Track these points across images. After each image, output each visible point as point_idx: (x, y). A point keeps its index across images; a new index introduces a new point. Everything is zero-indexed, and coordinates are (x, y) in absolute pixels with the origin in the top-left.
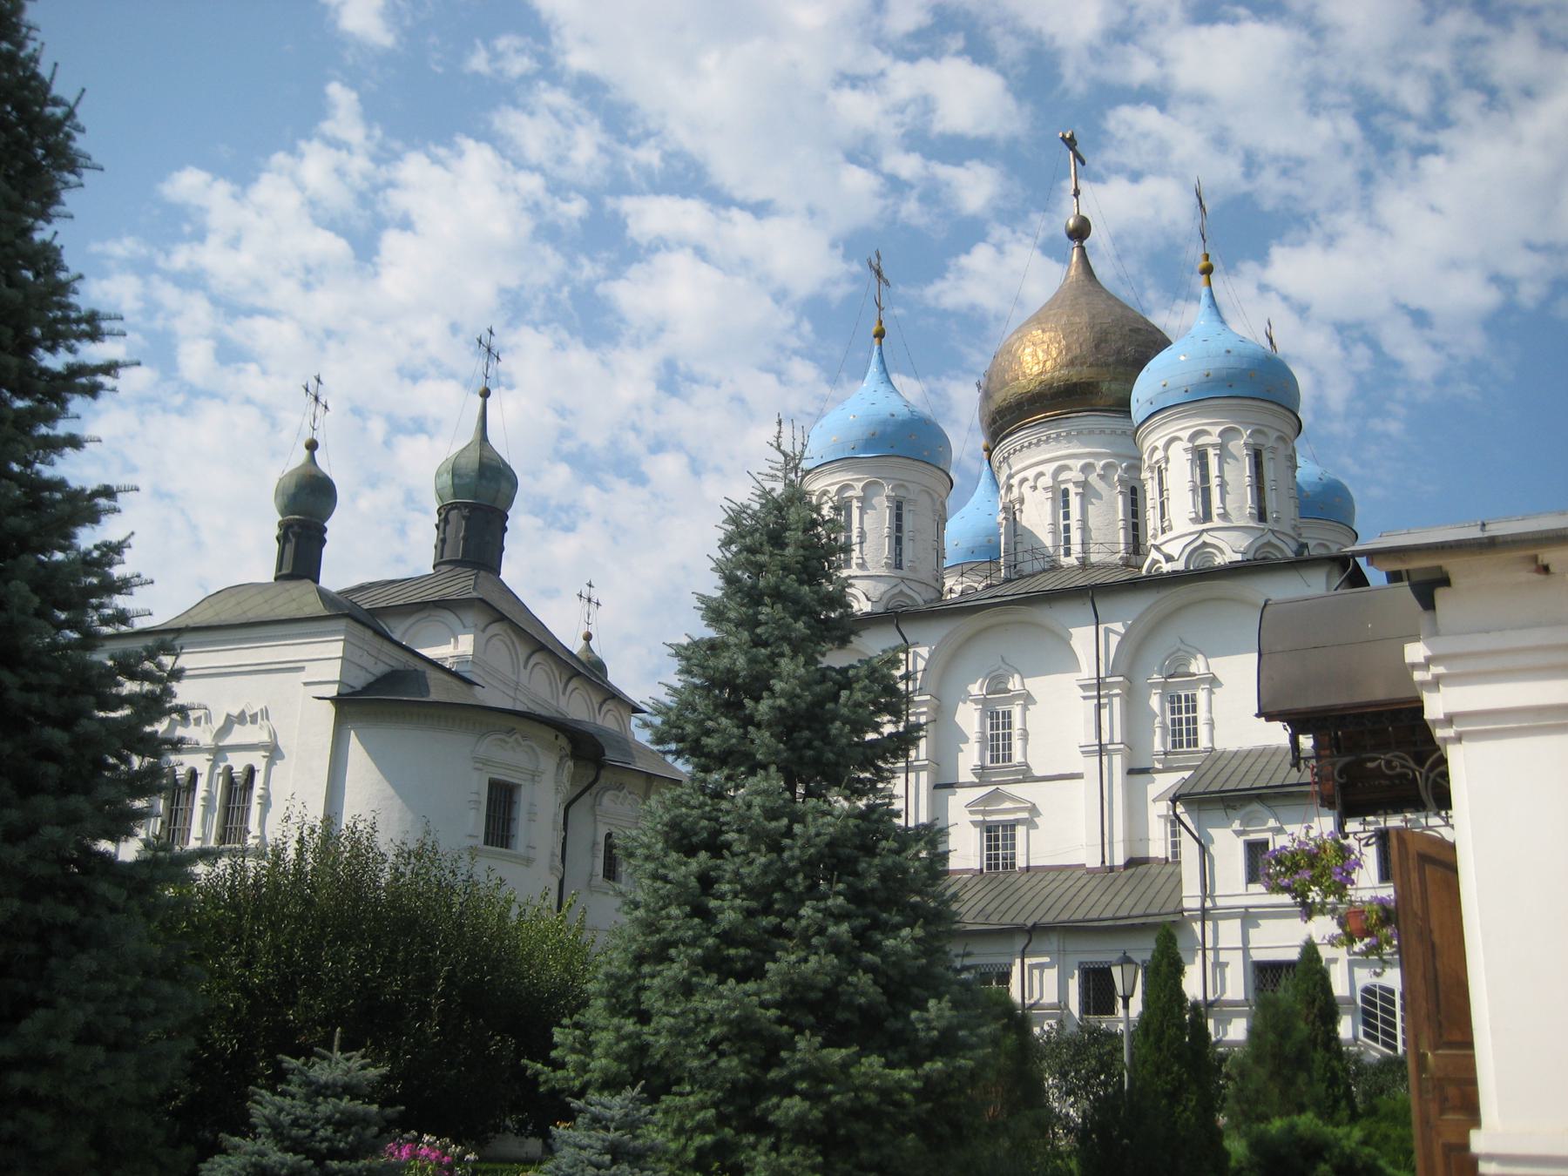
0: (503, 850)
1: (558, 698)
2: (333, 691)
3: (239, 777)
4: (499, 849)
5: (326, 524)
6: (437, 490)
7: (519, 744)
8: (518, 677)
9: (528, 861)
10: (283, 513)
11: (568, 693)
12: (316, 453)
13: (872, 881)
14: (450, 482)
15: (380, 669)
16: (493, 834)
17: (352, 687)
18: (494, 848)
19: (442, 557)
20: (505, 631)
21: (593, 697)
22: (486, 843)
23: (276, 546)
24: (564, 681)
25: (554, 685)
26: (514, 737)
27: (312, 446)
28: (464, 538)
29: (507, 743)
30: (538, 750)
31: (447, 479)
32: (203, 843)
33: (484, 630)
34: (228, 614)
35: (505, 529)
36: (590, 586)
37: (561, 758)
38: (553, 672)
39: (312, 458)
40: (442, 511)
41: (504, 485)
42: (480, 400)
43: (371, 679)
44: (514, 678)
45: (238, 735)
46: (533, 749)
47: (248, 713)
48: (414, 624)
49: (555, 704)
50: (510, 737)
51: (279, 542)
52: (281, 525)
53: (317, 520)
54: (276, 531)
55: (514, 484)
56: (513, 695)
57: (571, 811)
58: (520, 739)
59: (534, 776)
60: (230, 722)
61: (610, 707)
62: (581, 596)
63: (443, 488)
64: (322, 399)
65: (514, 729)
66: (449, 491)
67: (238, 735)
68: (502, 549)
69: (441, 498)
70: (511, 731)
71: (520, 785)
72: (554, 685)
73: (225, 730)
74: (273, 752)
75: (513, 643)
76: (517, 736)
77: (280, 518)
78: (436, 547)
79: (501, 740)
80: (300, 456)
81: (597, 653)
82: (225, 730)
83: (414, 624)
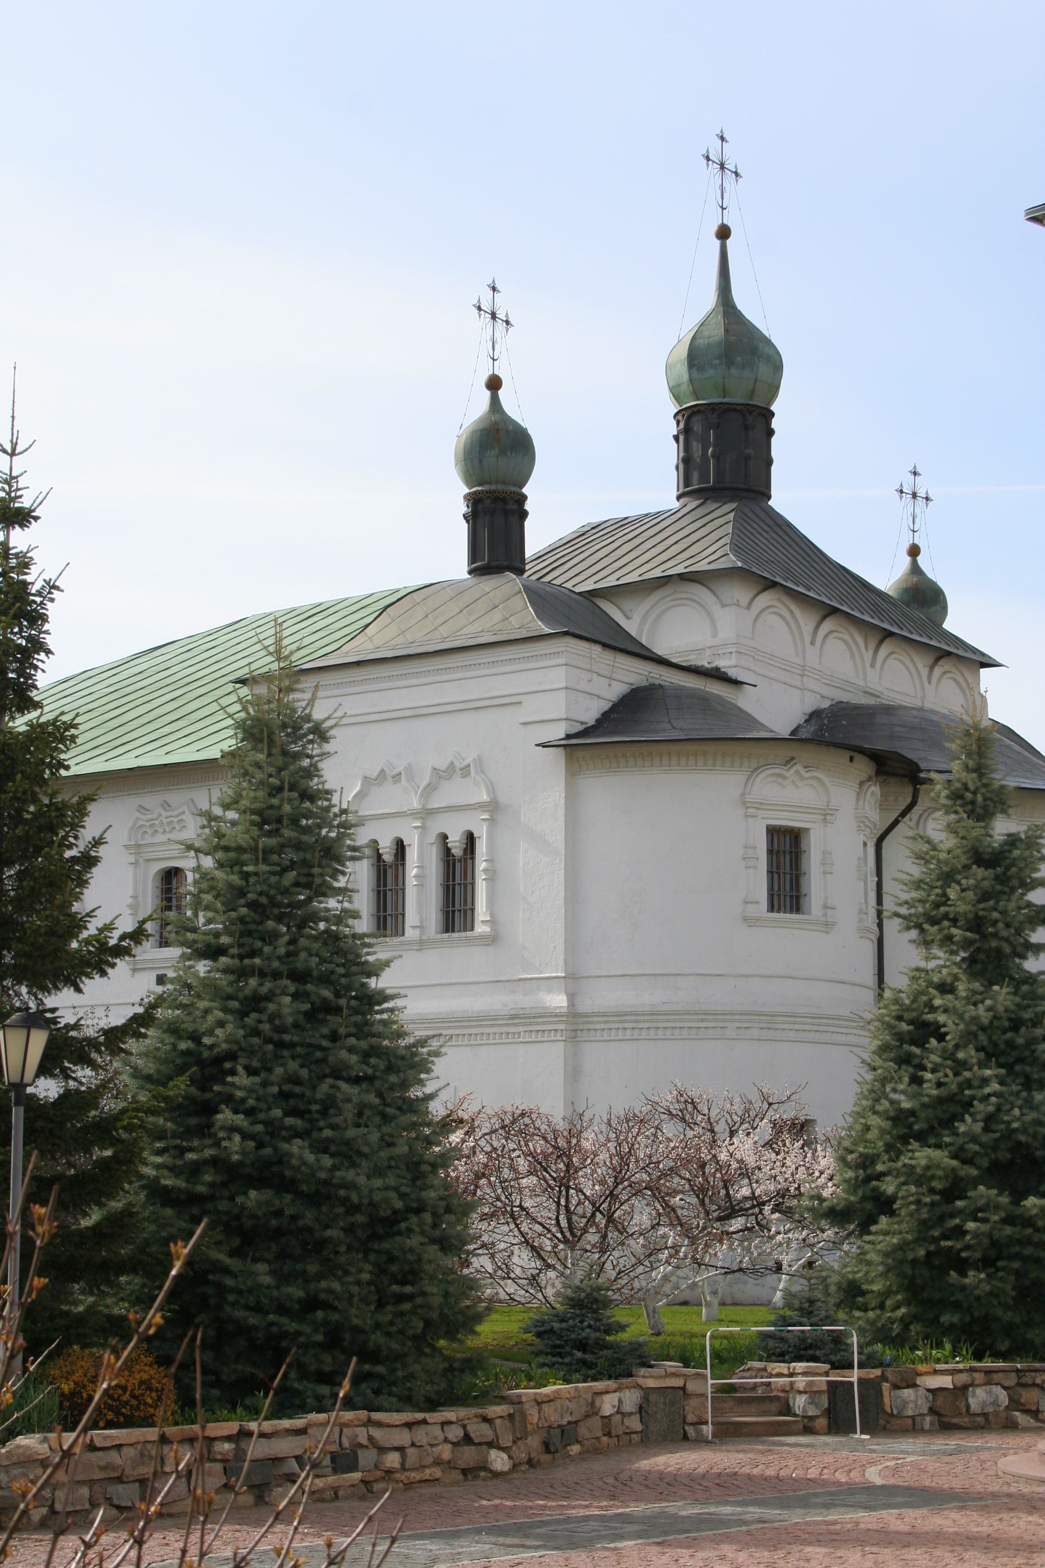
0: (794, 916)
1: (865, 674)
2: (558, 732)
3: (455, 847)
4: (788, 916)
5: (525, 490)
6: (671, 389)
7: (803, 778)
8: (804, 658)
9: (827, 926)
10: (469, 483)
11: (878, 664)
12: (501, 393)
13: (1020, 1041)
14: (686, 377)
15: (615, 691)
16: (779, 895)
17: (582, 723)
18: (781, 915)
19: (686, 485)
20: (780, 600)
21: (917, 660)
22: (771, 908)
23: (463, 528)
24: (871, 652)
25: (857, 655)
26: (793, 770)
27: (494, 384)
28: (713, 455)
29: (785, 778)
30: (826, 780)
31: (682, 371)
32: (422, 933)
33: (749, 606)
34: (420, 639)
35: (771, 433)
36: (915, 473)
37: (862, 783)
38: (856, 644)
39: (495, 402)
40: (680, 417)
41: (763, 371)
42: (718, 243)
43: (606, 706)
44: (799, 661)
45: (454, 793)
46: (823, 784)
47: (458, 765)
48: (655, 604)
49: (862, 683)
50: (788, 770)
51: (468, 522)
52: (468, 498)
53: (513, 489)
54: (463, 508)
55: (776, 366)
56: (798, 684)
57: (885, 844)
58: (802, 771)
59: (827, 815)
60: (442, 775)
61: (947, 668)
62: (901, 492)
63: (679, 385)
64: (501, 315)
65: (793, 758)
66: (686, 388)
67: (454, 793)
68: (769, 462)
69: (677, 398)
70: (790, 761)
71: (807, 830)
72: (857, 655)
73: (430, 789)
74: (493, 808)
75: (791, 612)
76: (798, 767)
77: (466, 490)
78: (677, 468)
79: (779, 775)
80: (480, 404)
81: (930, 575)
82: (430, 789)
83: (655, 604)
